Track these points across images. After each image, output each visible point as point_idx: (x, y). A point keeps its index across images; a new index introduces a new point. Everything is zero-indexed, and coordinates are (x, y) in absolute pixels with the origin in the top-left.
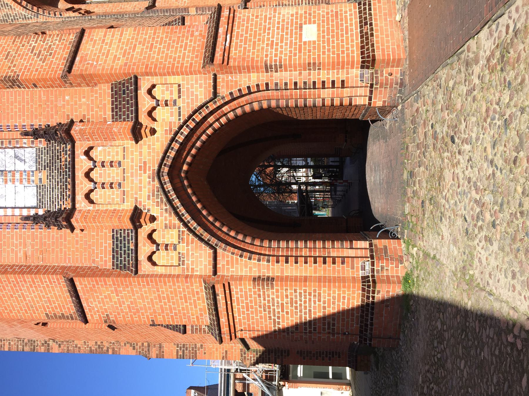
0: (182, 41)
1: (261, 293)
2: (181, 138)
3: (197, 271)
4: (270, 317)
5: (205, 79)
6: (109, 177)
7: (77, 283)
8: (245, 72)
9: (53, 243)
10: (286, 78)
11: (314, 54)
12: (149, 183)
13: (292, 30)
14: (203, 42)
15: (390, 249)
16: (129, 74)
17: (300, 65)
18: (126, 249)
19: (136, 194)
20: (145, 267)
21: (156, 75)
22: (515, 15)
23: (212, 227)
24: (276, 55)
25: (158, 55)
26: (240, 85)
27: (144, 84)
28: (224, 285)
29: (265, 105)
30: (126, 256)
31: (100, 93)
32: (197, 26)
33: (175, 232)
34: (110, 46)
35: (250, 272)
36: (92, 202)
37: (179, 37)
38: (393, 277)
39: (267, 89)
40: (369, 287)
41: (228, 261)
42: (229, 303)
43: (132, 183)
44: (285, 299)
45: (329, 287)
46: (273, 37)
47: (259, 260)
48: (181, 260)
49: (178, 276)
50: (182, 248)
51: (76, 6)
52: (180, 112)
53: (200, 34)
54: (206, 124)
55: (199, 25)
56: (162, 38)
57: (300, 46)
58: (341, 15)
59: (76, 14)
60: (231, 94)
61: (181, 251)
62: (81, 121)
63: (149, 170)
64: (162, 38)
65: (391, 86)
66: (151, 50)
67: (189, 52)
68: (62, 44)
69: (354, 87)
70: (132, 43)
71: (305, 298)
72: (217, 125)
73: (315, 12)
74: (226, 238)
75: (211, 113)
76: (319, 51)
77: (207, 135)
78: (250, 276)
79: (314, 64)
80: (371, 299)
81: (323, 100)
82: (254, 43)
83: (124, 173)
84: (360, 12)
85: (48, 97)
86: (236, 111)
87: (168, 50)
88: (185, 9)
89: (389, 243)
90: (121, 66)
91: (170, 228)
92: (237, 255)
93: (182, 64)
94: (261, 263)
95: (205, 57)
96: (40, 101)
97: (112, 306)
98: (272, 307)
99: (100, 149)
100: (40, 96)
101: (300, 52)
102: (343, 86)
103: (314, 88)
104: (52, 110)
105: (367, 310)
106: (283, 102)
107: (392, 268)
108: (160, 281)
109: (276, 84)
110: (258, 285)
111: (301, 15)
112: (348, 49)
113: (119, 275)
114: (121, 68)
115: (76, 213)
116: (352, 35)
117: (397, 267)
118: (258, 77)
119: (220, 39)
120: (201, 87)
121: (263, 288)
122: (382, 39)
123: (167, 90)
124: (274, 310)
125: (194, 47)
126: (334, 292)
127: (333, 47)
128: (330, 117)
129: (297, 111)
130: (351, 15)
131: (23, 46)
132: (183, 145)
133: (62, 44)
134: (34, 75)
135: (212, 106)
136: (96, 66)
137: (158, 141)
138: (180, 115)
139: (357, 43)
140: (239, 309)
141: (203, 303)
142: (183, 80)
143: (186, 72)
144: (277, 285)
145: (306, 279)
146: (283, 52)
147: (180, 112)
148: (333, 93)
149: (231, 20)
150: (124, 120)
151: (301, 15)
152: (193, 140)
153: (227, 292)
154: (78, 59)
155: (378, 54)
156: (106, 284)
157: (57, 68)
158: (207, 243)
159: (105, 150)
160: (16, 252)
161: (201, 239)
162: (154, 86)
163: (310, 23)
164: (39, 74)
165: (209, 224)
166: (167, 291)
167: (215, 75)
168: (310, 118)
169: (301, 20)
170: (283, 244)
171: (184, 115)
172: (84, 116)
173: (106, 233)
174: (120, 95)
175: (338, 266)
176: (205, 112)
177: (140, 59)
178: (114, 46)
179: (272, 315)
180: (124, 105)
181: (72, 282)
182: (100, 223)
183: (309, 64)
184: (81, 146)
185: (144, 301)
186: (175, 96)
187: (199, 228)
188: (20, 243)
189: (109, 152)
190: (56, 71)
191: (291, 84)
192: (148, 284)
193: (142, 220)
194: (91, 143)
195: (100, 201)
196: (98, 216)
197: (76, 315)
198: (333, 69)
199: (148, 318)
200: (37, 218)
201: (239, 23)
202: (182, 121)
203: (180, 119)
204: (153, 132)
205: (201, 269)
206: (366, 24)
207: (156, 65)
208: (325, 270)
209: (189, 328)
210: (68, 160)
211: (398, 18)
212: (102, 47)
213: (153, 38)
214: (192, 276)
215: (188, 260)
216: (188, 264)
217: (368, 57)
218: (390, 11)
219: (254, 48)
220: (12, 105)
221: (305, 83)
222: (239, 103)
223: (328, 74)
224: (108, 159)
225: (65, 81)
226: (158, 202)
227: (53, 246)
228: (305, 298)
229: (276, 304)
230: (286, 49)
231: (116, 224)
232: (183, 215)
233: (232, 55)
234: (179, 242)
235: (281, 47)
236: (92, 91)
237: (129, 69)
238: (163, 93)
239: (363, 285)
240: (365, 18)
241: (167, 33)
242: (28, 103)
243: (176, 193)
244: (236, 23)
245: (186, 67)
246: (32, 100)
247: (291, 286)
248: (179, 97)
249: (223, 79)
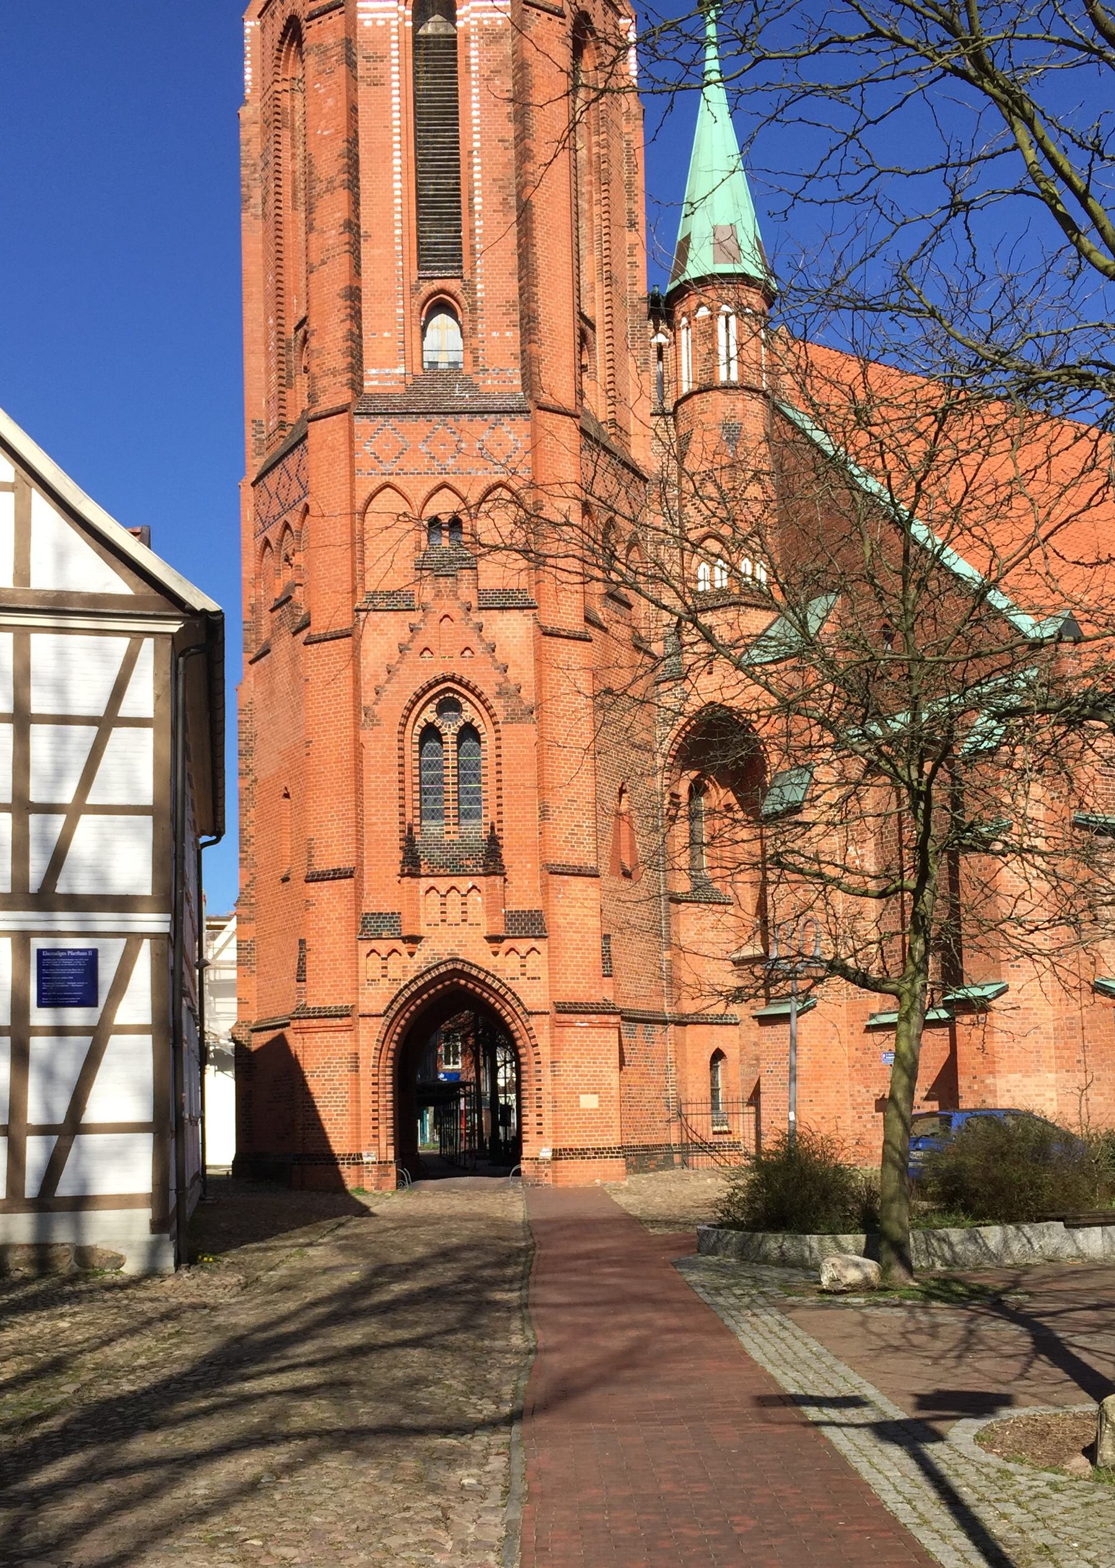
2: (489, 980)
33: (398, 974)
61: (380, 982)
105: (330, 1160)
119: (583, 1017)
132: (483, 982)
135: (519, 1010)
141: (331, 1003)
158: (389, 1007)
161: (392, 1002)
170: (389, 1079)
176: (514, 1003)
178: (580, 911)
194: (484, 892)
195: (428, 901)
196: (413, 901)
204: (495, 954)
209: (303, 984)
231: (406, 919)
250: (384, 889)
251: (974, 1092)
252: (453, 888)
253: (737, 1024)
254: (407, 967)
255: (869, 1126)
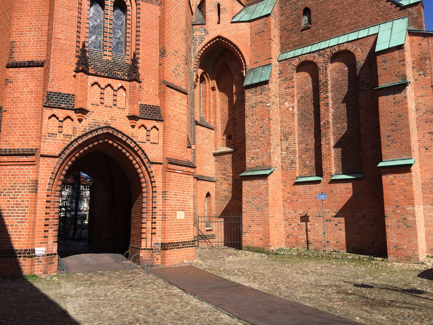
0: (179, 147)
1: (26, 185)
2: (128, 142)
3: (44, 144)
4: (5, 189)
5: (160, 158)
6: (107, 97)
7: (39, 68)
8: (163, 180)
9: (67, 57)
10: (158, 202)
11: (170, 218)
12: (103, 121)
13: (182, 205)
14: (178, 158)
15: (52, 266)
16: (165, 117)
17: (165, 210)
18: (61, 102)
19: (97, 112)
20: (48, 112)
21: (163, 132)
22: (187, 297)
23: (72, 155)
24: (170, 197)
25: (174, 134)
26: (156, 177)
27: (159, 125)
28: (35, 161)
29: (144, 190)
30: (56, 101)
31: (155, 100)
32: (186, 155)
33: (70, 132)
34: (178, 108)
35: (41, 178)
36: (93, 85)
37: (181, 145)
38: (34, 268)
39: (153, 192)
40: (28, 253)
41: (50, 164)
42: (19, 163)
43: (103, 111)
44: (20, 200)
45: (29, 229)
46: (179, 195)
47: (49, 184)
48: (51, 135)
49: (41, 133)
50: (60, 137)
51: (199, 80)
52: (143, 142)
53: (182, 157)
54: (136, 156)
55: (187, 157)
56: (181, 136)
57: (174, 210)
58: (188, 232)
59: (195, 80)
60: (152, 172)
61: (58, 135)
62: (140, 87)
63: (111, 122)
64: (181, 136)
65: (151, 260)
66: (176, 130)
67: (174, 150)
68: (181, 82)
69: (152, 239)
70: (180, 120)
71: (21, 213)
72: (134, 162)
73: (190, 218)
74: (65, 164)
75: (142, 160)
76: (172, 220)
77: (129, 156)
78: (38, 178)
79: (165, 218)
80: (19, 255)
81: (145, 223)
82: (177, 186)
83: (109, 107)
84: (189, 242)
85: (154, 70)
86: (142, 174)
87: (176, 139)
88: (195, 143)
89: (55, 266)
90: (169, 114)
91: (73, 130)
92: (54, 170)
93: (168, 146)
94: (47, 185)
95: (171, 159)
96: (152, 66)
97: (20, 87)
98: (14, 191)
99: (124, 94)
100: (154, 66)
101: (172, 210)
102: (152, 234)
103: (152, 218)
104: (147, 71)
106: (145, 200)
107: (40, 268)
108: (38, 121)
109: (156, 197)
110: (32, 183)
111: (189, 210)
112: (172, 235)
113: (44, 95)
114: (168, 113)
115: (86, 76)
116: (178, 238)
117: (41, 271)
118: (160, 187)
119: (180, 167)
120: (156, 155)
121: (30, 186)
122: (176, 254)
123: (155, 137)
124: (12, 192)
125: (176, 153)
126: (24, 232)
127: (173, 228)
128: (132, 227)
129: (139, 208)
130: (188, 237)
131: (181, 61)
132: (125, 142)
133: (181, 82)
134: (166, 66)
135: (145, 161)
136: (169, 100)
137: (127, 128)
138: (141, 142)
139: (174, 240)
140: (14, 169)
141: (18, 146)
142: (160, 146)
143: (165, 148)
144: (31, 195)
145: (35, 213)
146: (172, 201)
147: (143, 142)
148: (149, 228)
149: (188, 173)
150: (140, 111)
151: (189, 210)
152: (127, 148)
153: (29, 163)
154: (173, 90)
155: (168, 252)
156: (38, 86)
157: (169, 79)
158: (63, 152)
159: (123, 97)
160: (62, 34)
161: (65, 149)
162: (157, 129)
163: (185, 215)
164: (166, 68)
165: (74, 154)
166: (30, 124)
167: (162, 164)
168: (132, 215)
169: (187, 210)
171: (141, 145)
172: (143, 89)
173: (72, 90)
174: (154, 111)
175: (42, 234)
176: (143, 157)
177: (172, 124)
179: (7, 191)
180: (148, 112)
181: (42, 66)
182: (80, 89)
183: (165, 215)
184: (127, 85)
185: (22, 108)
186: (152, 141)
187: (73, 148)
188: (68, 37)
189: (122, 100)
190: (167, 78)
191: (155, 205)
192: (36, 113)
193: (80, 114)
194: (128, 90)
196: (84, 88)
197: (12, 60)
198: (162, 228)
199: (8, 108)
200: (84, 52)
201: (187, 177)
202: (138, 143)
203: (139, 142)
204: (133, 127)
205: (45, 147)
206: (183, 245)
207: (168, 132)
208: (40, 225)
210: (119, 76)
211: (185, 261)
212: (178, 103)
213: (181, 131)
214: (40, 141)
215: (51, 139)
216: (49, 139)
217: (167, 247)
218: (189, 257)
219: (175, 185)
220: (151, 49)
221: (155, 213)
222: (146, 175)
223: (160, 225)
224: (118, 99)
225: (162, 82)
226: (91, 125)
227: (65, 57)
228: (21, 213)
229: (16, 194)
230: (173, 203)
231: (79, 98)
232: (82, 139)
233: (172, 174)
234: (64, 135)
235: (174, 200)
236: (156, 95)
237: (167, 118)
238: (154, 134)
239: (30, 250)
240: (186, 245)
241: (184, 139)
242: (151, 58)
243: (96, 136)
244: (187, 176)
245: (167, 149)
246: (153, 61)
247: (31, 204)
248: (151, 143)
249: (160, 168)
250: (63, 77)
251: (397, 214)
252: (109, 85)
253: (215, 182)
254: (76, 129)
255: (296, 229)
